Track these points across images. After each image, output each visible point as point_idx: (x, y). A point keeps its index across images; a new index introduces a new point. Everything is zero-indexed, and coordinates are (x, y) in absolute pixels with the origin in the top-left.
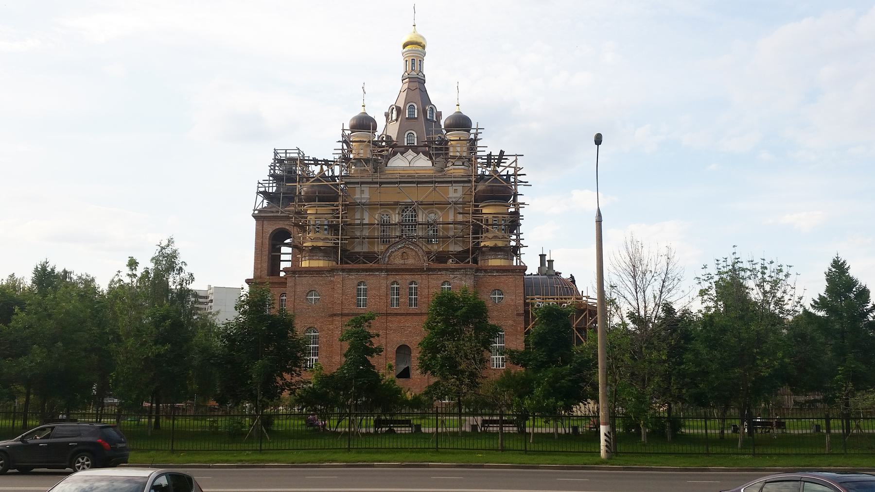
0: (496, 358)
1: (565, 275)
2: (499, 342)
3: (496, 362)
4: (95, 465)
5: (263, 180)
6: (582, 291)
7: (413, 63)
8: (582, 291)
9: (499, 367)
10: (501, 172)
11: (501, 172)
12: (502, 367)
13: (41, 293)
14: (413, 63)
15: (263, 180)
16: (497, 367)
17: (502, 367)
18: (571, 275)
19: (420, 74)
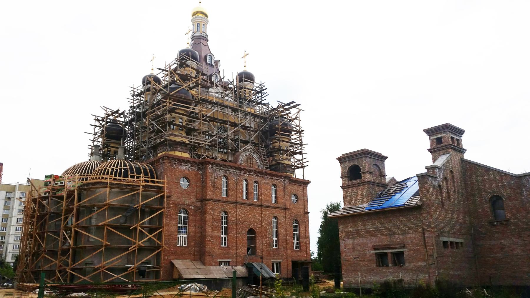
0: (181, 237)
1: (24, 182)
2: (181, 228)
3: (181, 240)
4: (75, 192)
5: (104, 107)
6: (228, 80)
7: (198, 28)
8: (228, 80)
9: (182, 245)
10: (255, 83)
11: (255, 83)
12: (184, 245)
13: (510, 223)
14: (198, 26)
15: (104, 107)
16: (180, 245)
17: (184, 245)
18: (94, 120)
19: (204, 33)
